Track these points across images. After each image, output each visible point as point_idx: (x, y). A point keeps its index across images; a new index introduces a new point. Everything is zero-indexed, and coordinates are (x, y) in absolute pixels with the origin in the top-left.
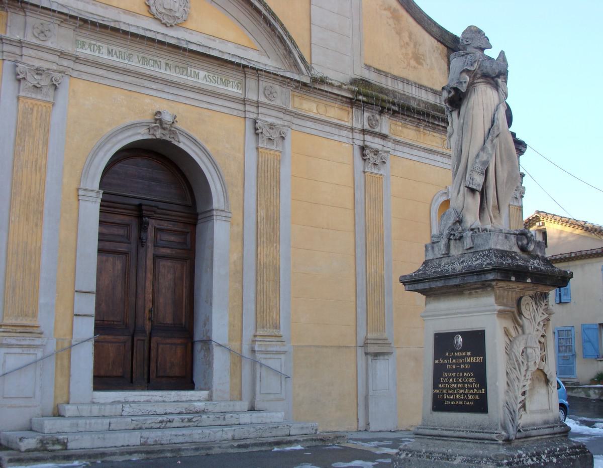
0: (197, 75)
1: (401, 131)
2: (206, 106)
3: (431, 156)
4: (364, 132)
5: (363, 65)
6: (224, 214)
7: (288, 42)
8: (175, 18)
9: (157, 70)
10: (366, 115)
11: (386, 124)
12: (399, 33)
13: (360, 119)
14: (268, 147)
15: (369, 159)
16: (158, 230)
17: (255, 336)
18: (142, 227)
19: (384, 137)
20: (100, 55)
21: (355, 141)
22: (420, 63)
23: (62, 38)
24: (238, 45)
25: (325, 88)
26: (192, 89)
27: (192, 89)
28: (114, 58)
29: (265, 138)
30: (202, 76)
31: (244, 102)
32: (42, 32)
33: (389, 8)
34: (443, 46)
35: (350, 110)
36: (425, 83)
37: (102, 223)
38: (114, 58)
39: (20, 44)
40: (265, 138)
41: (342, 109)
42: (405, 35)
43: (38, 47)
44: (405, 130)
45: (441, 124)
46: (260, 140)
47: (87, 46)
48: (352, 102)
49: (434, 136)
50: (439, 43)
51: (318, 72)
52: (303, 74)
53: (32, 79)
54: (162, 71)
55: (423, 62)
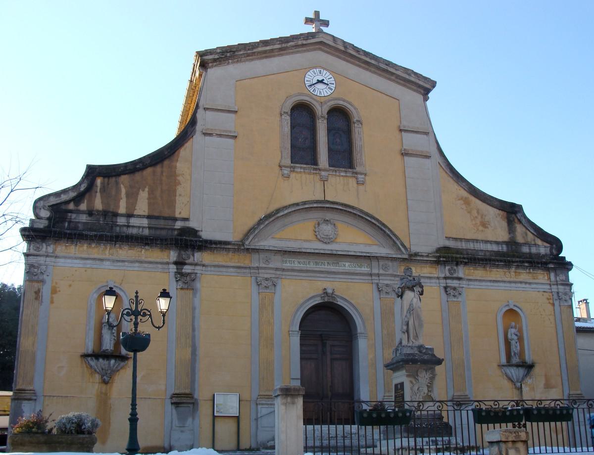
0: (345, 266)
1: (473, 272)
2: (350, 280)
3: (496, 284)
4: (446, 278)
5: (445, 238)
6: (363, 335)
7: (393, 238)
8: (330, 239)
9: (323, 267)
10: (447, 268)
11: (461, 271)
12: (469, 212)
13: (445, 271)
14: (386, 296)
15: (450, 293)
16: (332, 346)
17: (384, 396)
18: (324, 345)
19: (459, 279)
20: (294, 265)
21: (441, 284)
22: (486, 227)
23: (276, 262)
24: (366, 245)
25: (418, 258)
26: (342, 273)
27: (342, 273)
28: (302, 265)
29: (384, 292)
30: (347, 266)
31: (371, 275)
32: (267, 261)
33: (462, 199)
34: (503, 212)
35: (437, 266)
36: (490, 239)
37: (301, 345)
38: (302, 265)
39: (258, 268)
40: (384, 292)
41: (432, 267)
42: (475, 213)
43: (265, 268)
44: (476, 272)
45: (500, 264)
46: (381, 294)
47: (288, 262)
48: (438, 262)
49: (497, 271)
50: (500, 211)
51: (414, 249)
52: (403, 254)
53: (264, 283)
54: (326, 267)
55: (489, 226)
